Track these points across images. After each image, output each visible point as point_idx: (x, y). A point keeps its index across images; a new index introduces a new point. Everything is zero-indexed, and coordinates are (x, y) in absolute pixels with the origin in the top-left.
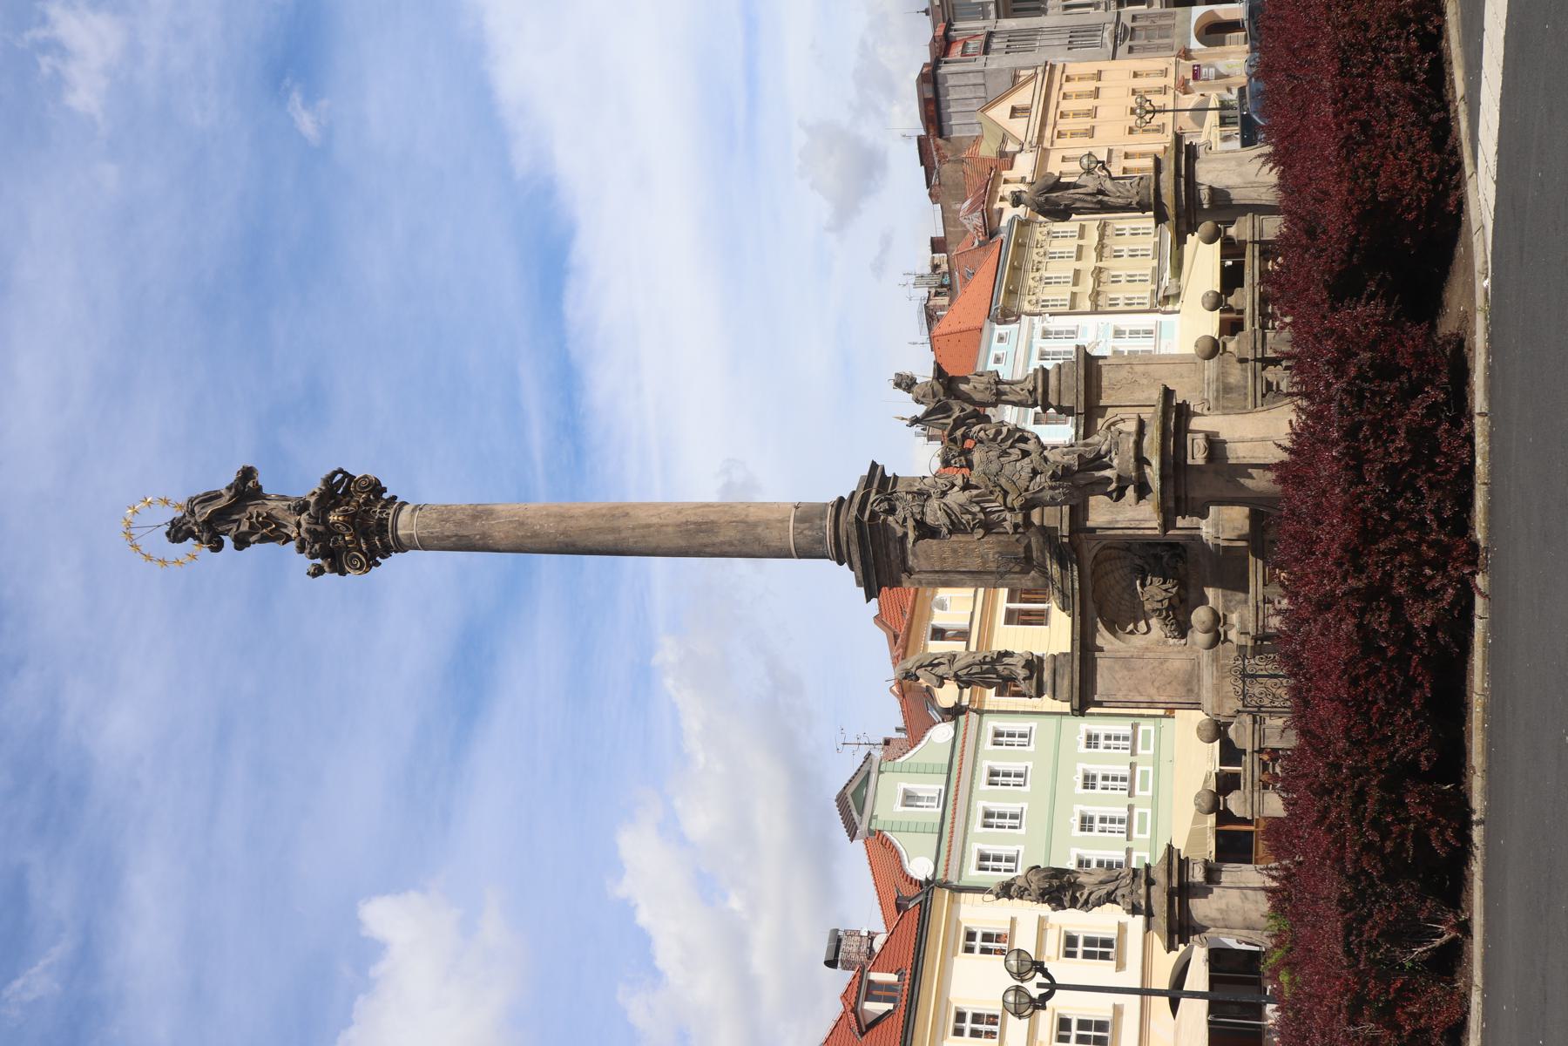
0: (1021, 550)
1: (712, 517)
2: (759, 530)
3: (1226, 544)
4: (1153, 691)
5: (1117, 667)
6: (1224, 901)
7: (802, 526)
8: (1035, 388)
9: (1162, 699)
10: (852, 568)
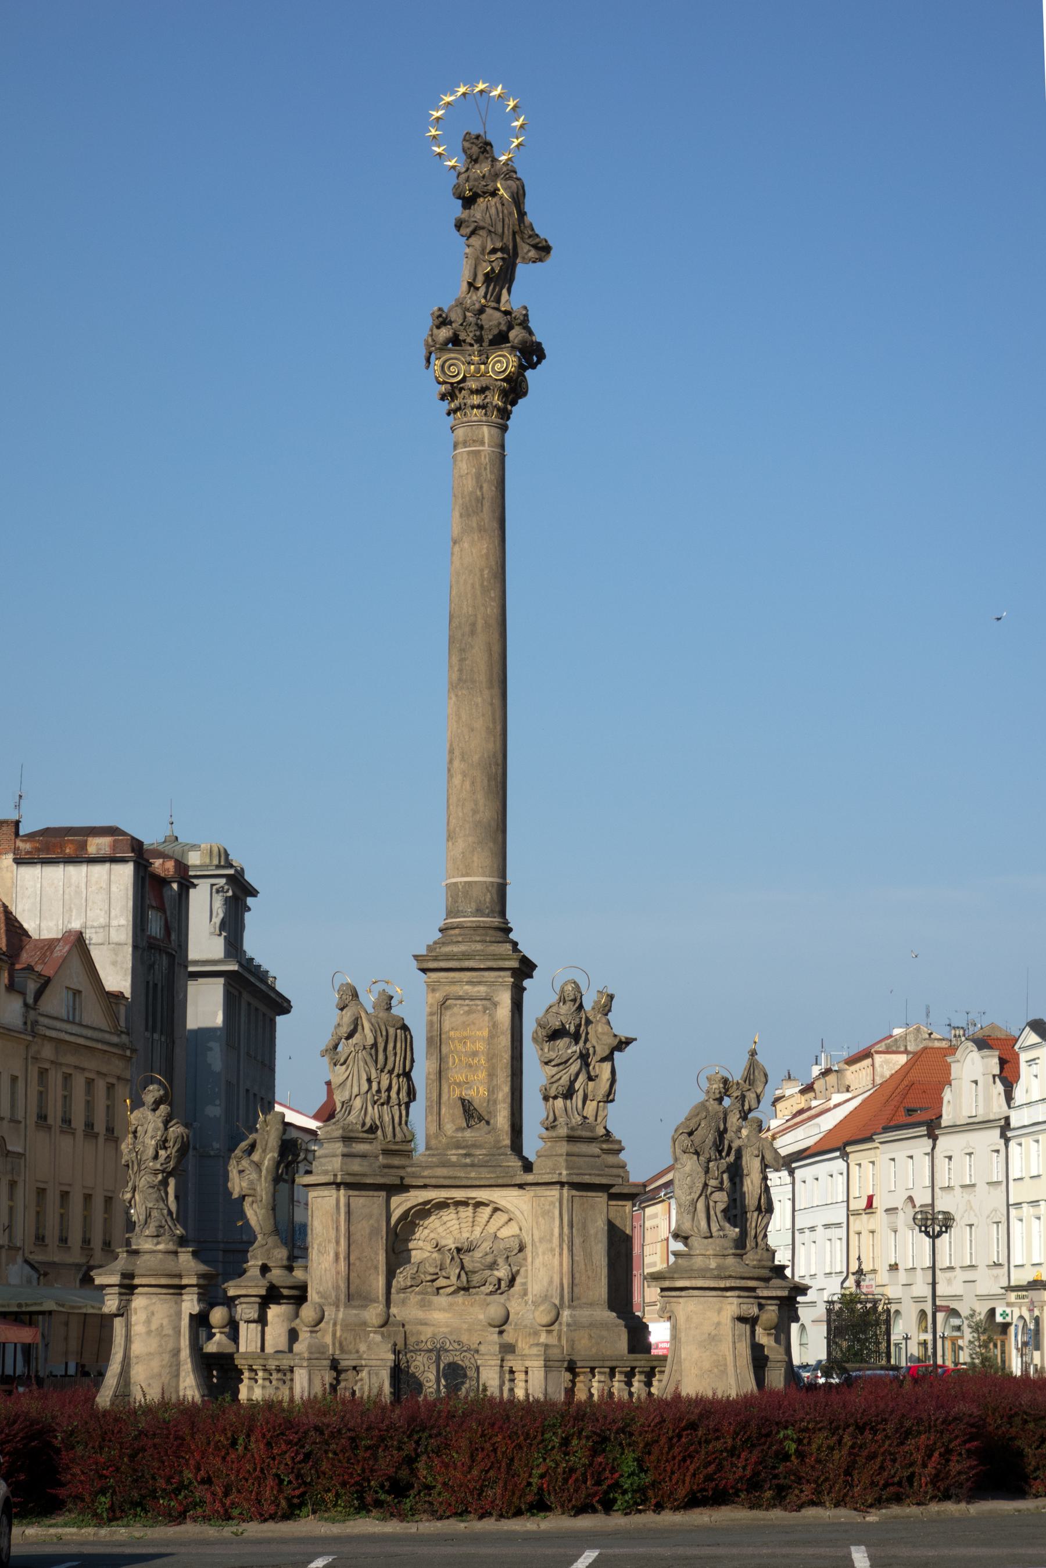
5: (372, 1222)
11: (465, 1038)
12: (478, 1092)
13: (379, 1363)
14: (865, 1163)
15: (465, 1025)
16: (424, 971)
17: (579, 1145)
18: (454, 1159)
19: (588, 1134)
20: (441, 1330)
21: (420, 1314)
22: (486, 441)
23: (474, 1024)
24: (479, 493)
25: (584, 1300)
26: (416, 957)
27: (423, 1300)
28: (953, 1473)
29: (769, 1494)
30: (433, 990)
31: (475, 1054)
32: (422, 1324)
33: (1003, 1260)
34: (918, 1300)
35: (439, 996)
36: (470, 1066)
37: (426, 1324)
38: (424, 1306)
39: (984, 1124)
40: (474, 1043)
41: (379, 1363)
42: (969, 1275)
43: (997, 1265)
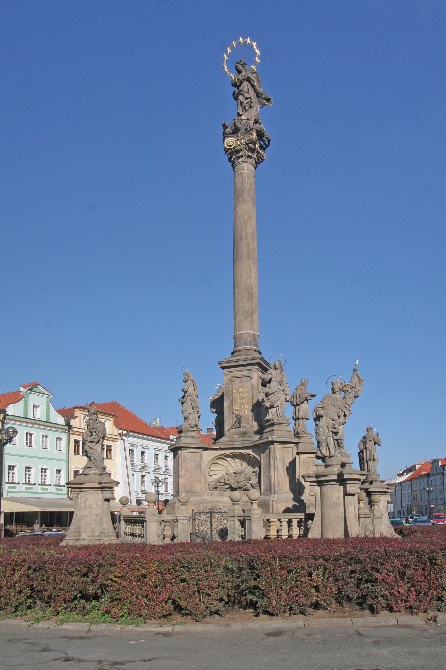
0: (244, 425)
1: (254, 299)
2: (250, 319)
3: (271, 505)
4: (187, 477)
5: (196, 463)
6: (95, 506)
7: (252, 336)
8: (305, 433)
9: (184, 481)
10: (231, 357)
11: (239, 392)
12: (245, 413)
13: (183, 518)
14: (415, 482)
15: (239, 387)
16: (223, 368)
17: (281, 426)
18: (235, 439)
19: (286, 422)
20: (227, 505)
21: (219, 499)
22: (245, 168)
23: (243, 386)
24: (242, 188)
25: (284, 491)
26: (219, 363)
27: (220, 493)
28: (256, 157)
29: (235, 569)
30: (227, 375)
31: (243, 398)
32: (219, 503)
33: (443, 498)
34: (425, 506)
35: (229, 377)
36: (242, 403)
37: (221, 503)
38: (221, 495)
39: (439, 474)
40: (243, 394)
41: (183, 518)
42: (436, 501)
43: (442, 499)
